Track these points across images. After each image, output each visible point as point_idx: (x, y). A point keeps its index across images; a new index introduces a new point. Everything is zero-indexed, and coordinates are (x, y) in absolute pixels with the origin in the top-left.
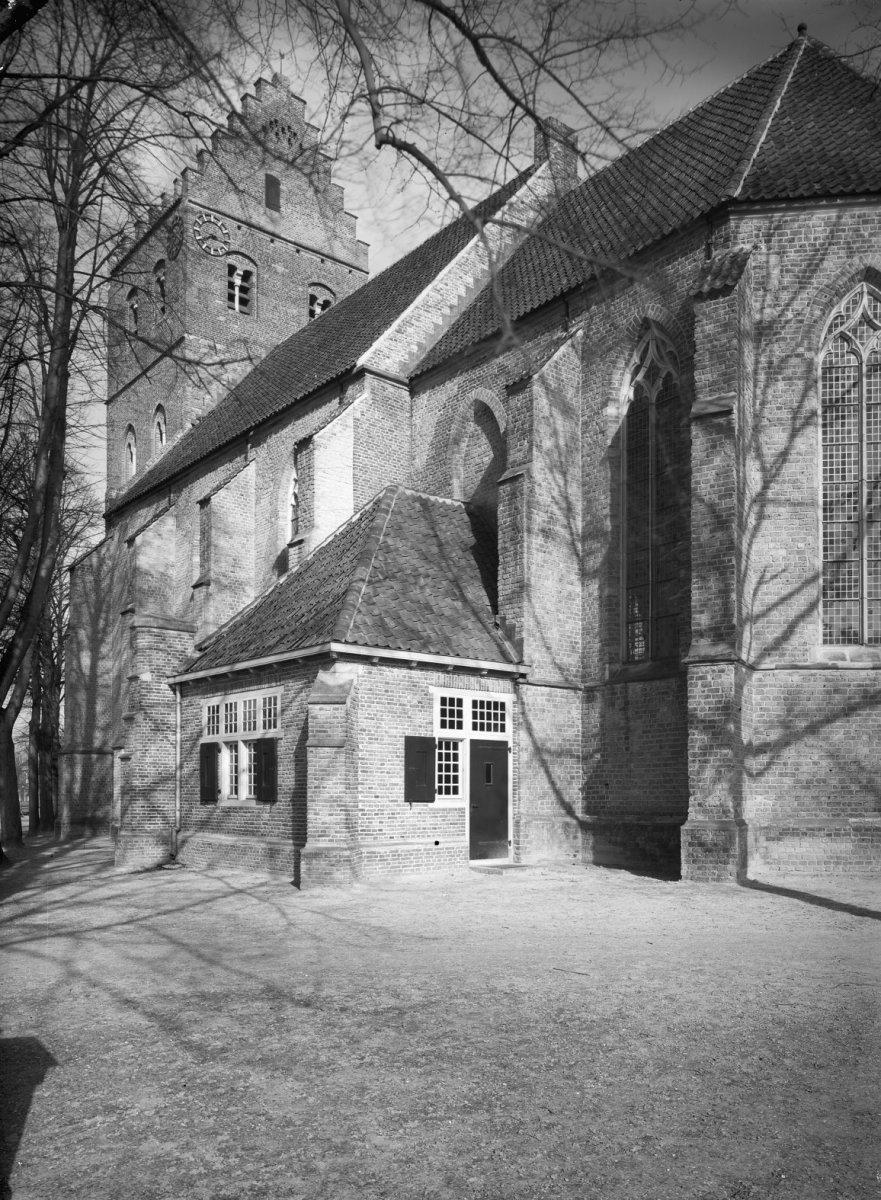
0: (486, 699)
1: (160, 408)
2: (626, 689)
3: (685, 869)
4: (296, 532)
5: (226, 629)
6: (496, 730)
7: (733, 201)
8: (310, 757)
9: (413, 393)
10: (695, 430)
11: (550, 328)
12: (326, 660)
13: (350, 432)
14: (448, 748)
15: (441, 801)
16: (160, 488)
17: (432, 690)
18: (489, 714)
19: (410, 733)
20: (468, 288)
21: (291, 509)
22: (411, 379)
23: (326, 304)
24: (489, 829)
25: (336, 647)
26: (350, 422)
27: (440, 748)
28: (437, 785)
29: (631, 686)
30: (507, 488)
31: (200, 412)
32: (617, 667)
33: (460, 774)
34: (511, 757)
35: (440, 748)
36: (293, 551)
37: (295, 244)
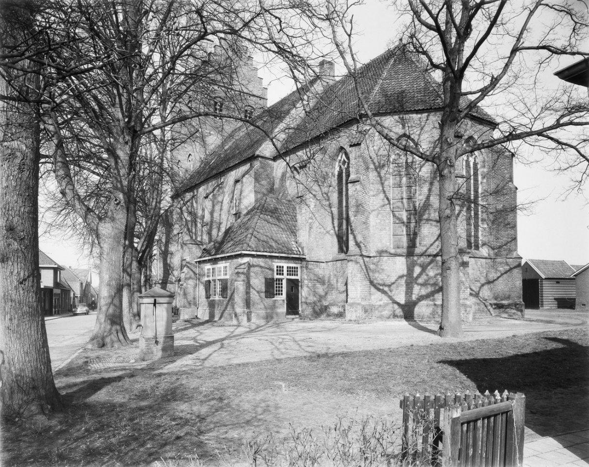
15: (277, 298)
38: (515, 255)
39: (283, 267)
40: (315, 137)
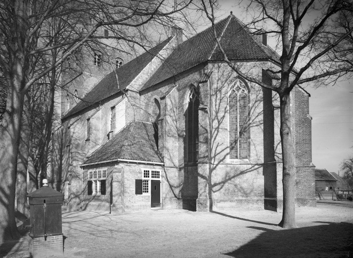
0: (155, 171)
1: (76, 90)
2: (188, 168)
3: (197, 208)
4: (111, 129)
5: (94, 153)
6: (157, 178)
7: (209, 60)
8: (113, 184)
9: (140, 95)
10: (199, 111)
11: (171, 83)
12: (117, 163)
13: (125, 105)
14: (146, 182)
15: (144, 194)
16: (77, 113)
17: (142, 169)
18: (156, 175)
19: (136, 179)
20: (154, 69)
21: (110, 122)
22: (140, 92)
23: (121, 63)
24: (156, 201)
25: (119, 159)
26: (125, 103)
27: (144, 182)
28: (143, 190)
29: (189, 167)
30: (160, 121)
31: (87, 92)
32: (186, 163)
33: (149, 188)
34: (161, 184)
35: (144, 182)
36: (111, 134)
37: (112, 47)
38: (311, 165)
39: (149, 171)
40: (180, 73)
